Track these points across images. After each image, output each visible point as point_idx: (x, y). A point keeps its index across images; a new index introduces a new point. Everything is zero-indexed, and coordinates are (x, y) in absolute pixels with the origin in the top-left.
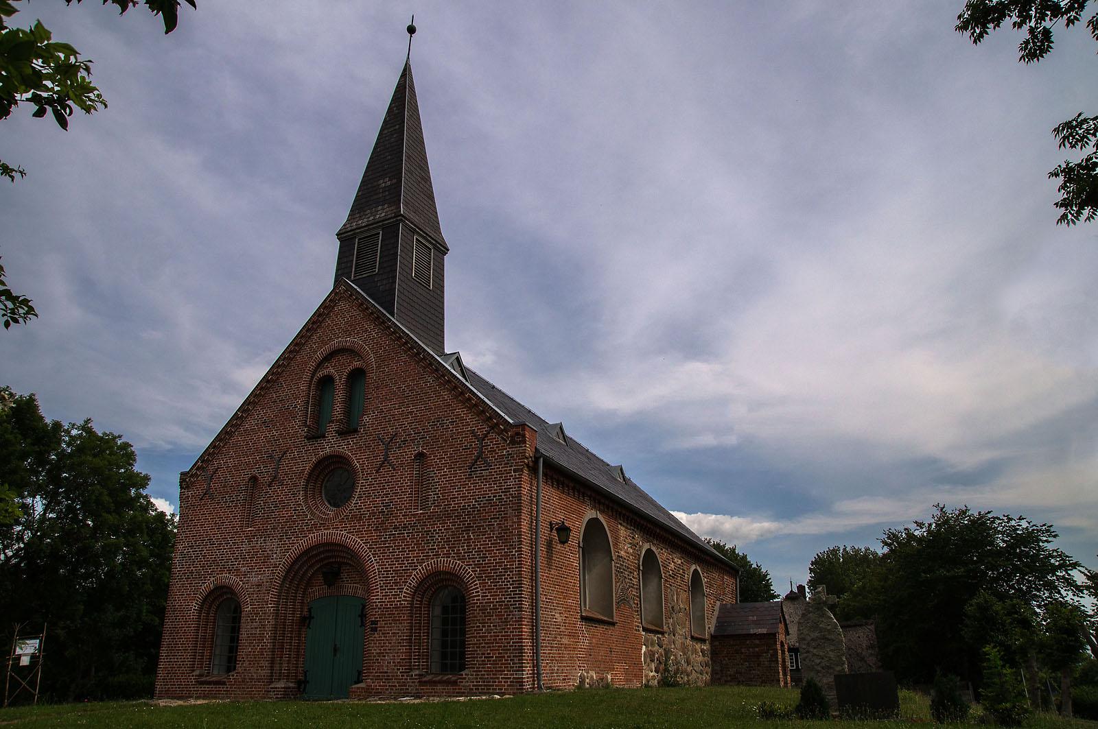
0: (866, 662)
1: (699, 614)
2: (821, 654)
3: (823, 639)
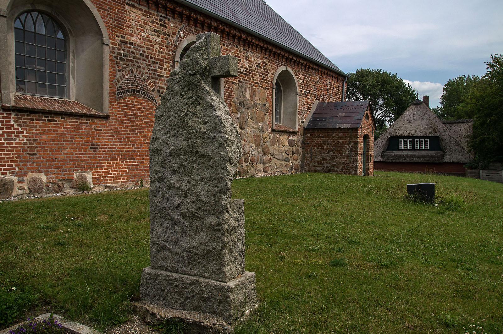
0: (461, 146)
1: (291, 110)
2: (184, 185)
3: (192, 153)
